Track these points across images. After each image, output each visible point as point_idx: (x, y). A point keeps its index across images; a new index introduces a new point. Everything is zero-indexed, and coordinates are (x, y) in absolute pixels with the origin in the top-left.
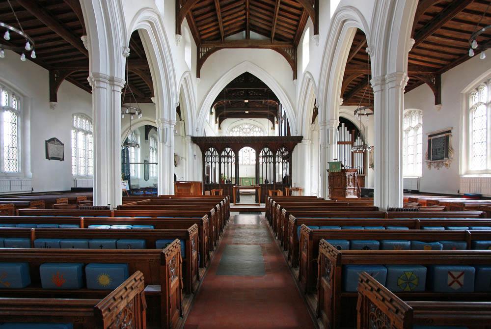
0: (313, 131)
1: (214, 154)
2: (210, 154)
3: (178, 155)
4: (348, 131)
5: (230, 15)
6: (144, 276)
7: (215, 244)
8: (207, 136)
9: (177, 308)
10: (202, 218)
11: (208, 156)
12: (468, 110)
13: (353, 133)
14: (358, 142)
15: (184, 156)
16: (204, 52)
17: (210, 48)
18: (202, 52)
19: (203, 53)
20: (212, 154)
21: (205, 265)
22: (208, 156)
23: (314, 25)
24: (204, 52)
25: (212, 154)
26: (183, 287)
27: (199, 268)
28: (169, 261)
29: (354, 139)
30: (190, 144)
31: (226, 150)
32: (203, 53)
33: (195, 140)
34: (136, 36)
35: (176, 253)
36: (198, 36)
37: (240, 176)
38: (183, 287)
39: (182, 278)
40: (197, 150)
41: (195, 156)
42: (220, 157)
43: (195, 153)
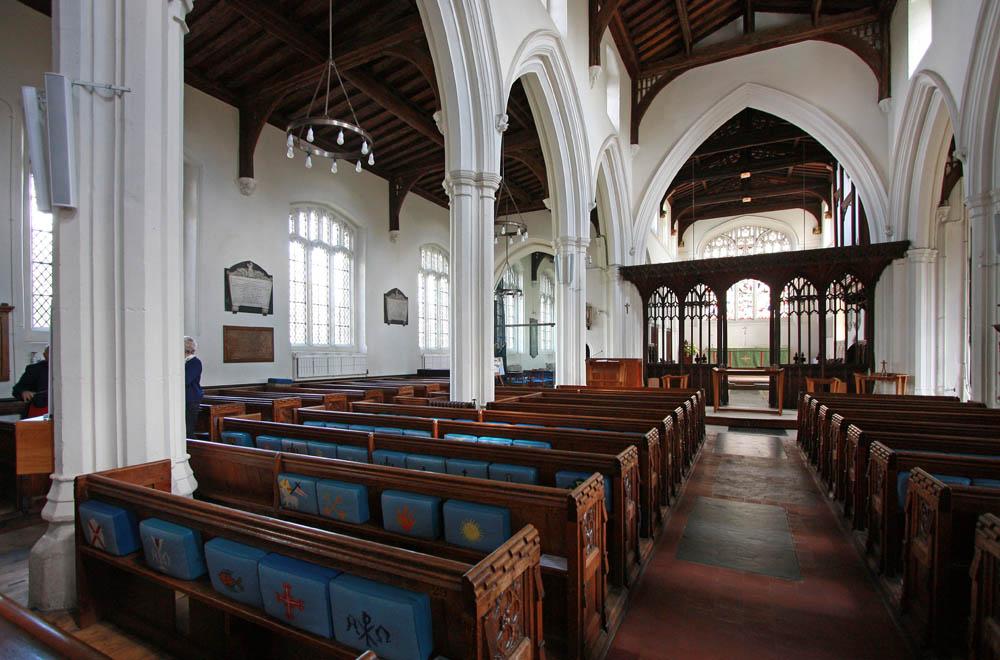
0: (943, 224)
16: (646, 88)
17: (659, 76)
19: (644, 92)
23: (881, 85)
25: (663, 299)
27: (640, 539)
28: (583, 513)
31: (695, 291)
32: (644, 92)
36: (633, 57)
37: (729, 347)
39: (606, 553)
41: (627, 306)
42: (682, 305)
43: (627, 301)
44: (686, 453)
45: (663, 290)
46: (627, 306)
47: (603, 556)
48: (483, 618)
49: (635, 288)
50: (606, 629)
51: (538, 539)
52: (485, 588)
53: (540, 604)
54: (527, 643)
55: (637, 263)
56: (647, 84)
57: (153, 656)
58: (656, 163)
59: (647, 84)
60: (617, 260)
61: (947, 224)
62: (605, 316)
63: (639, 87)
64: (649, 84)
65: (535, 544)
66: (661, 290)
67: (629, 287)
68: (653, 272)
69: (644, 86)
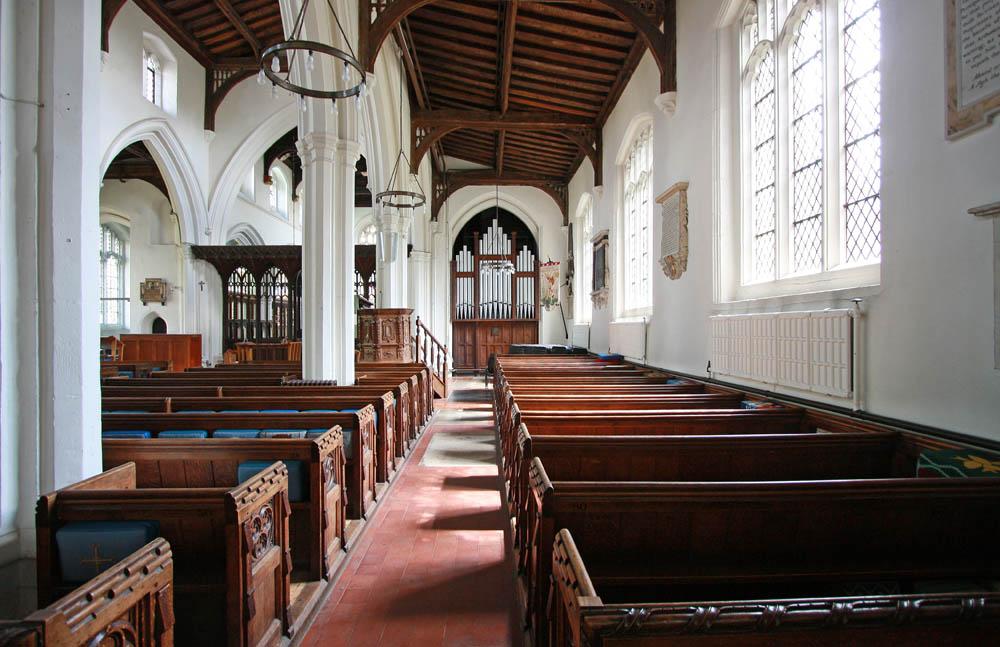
0: (433, 234)
1: (245, 280)
2: (270, 280)
3: (169, 281)
4: (505, 235)
5: (461, 42)
6: (287, 468)
7: (408, 445)
8: (200, 244)
9: (337, 535)
10: (382, 397)
11: (267, 285)
12: (737, 78)
13: (514, 238)
14: (525, 254)
15: (179, 285)
16: (222, 79)
17: (234, 72)
18: (218, 80)
19: (220, 83)
20: (242, 279)
21: (387, 477)
22: (267, 285)
24: (222, 79)
25: (242, 279)
26: (346, 503)
27: (376, 484)
28: (324, 458)
29: (517, 250)
30: (189, 260)
32: (220, 83)
33: (199, 252)
34: (971, 212)
35: (335, 446)
36: (196, 45)
38: (346, 503)
39: (345, 489)
40: (208, 273)
41: (201, 283)
43: (202, 279)
44: (412, 427)
45: (241, 271)
46: (201, 283)
47: (342, 491)
48: (243, 524)
49: (212, 266)
50: (345, 550)
51: (286, 472)
52: (244, 502)
53: (287, 519)
54: (276, 549)
55: (214, 243)
56: (222, 76)
57: (72, 489)
58: (230, 153)
59: (222, 76)
60: (190, 240)
61: (436, 235)
62: (180, 292)
63: (216, 77)
64: (225, 77)
65: (283, 474)
66: (239, 270)
67: (203, 264)
68: (222, 253)
69: (220, 77)
